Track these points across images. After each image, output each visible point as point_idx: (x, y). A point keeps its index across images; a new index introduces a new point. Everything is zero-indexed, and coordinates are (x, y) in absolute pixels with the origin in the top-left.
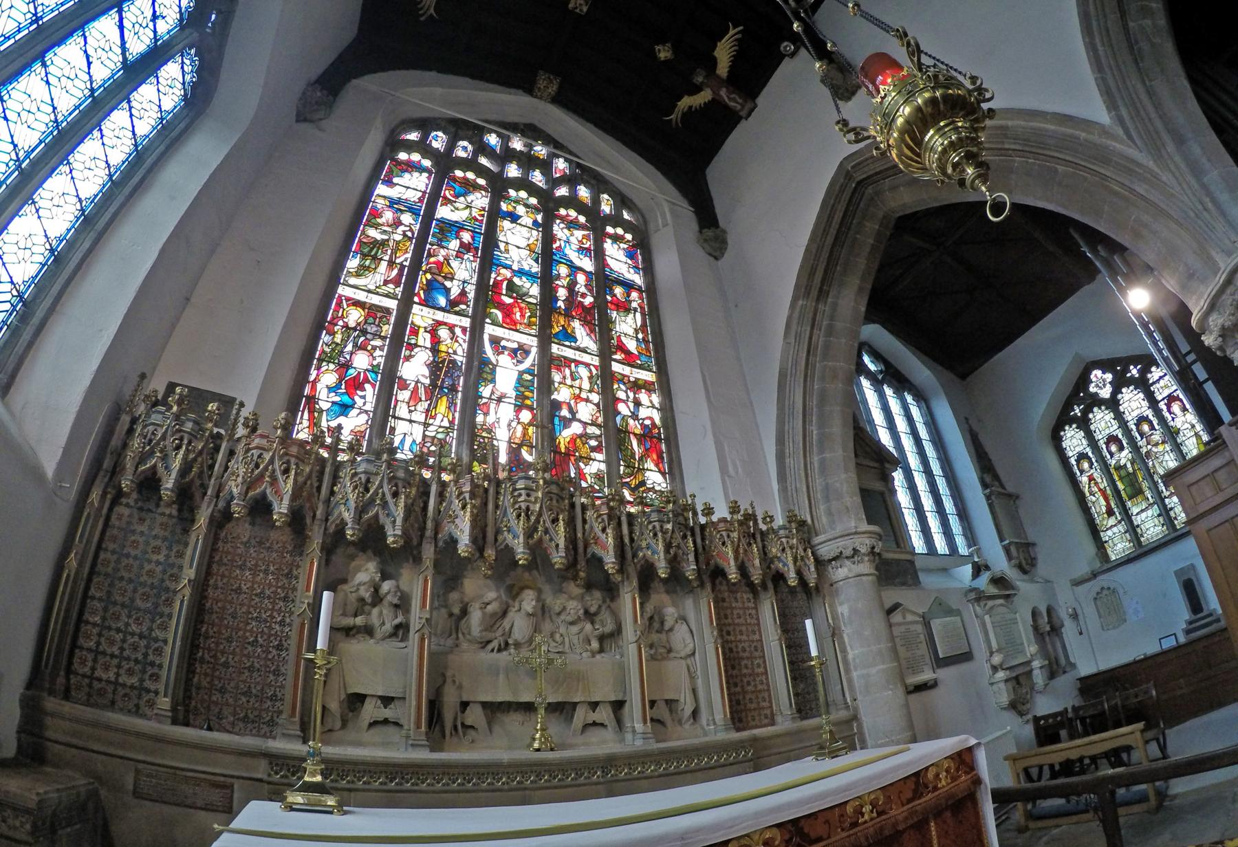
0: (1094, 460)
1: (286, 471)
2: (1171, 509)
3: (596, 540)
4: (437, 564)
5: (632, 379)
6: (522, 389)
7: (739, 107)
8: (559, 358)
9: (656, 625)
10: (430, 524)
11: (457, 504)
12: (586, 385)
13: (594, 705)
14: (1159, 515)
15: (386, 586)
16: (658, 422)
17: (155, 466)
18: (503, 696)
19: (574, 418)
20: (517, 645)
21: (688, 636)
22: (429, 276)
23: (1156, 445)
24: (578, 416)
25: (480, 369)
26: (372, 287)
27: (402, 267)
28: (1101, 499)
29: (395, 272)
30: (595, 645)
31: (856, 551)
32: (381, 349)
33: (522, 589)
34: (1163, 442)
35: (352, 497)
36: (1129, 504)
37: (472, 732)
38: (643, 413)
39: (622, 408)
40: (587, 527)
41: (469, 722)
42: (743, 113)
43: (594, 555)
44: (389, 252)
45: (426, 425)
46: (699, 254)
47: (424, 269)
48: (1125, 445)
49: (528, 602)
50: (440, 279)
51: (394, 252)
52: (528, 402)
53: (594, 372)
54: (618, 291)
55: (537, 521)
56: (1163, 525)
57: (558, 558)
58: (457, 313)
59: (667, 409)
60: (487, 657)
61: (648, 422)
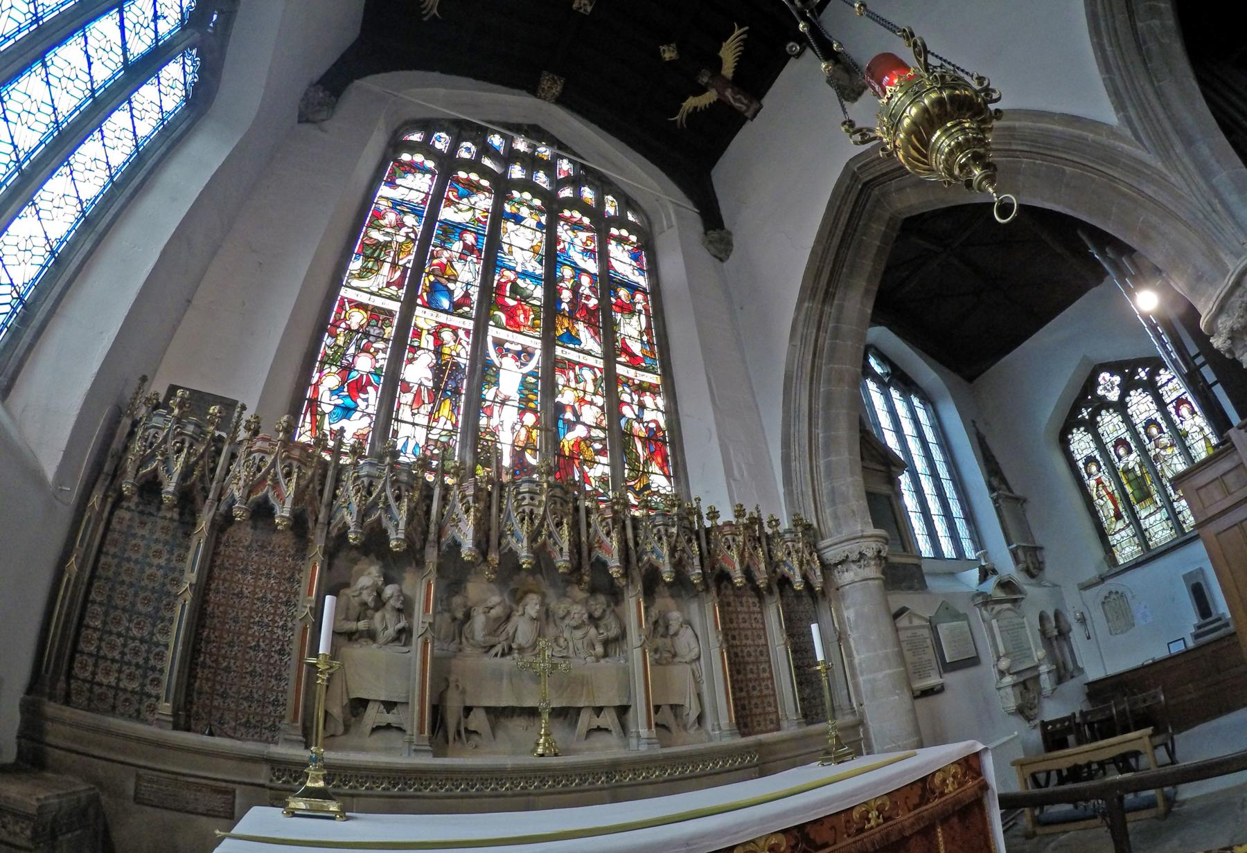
0: (1102, 463)
1: (288, 475)
2: (1180, 512)
3: (601, 543)
4: (440, 568)
5: (637, 382)
6: (526, 392)
7: (744, 108)
8: (563, 360)
9: (661, 630)
10: (433, 528)
11: (460, 507)
12: (590, 388)
13: (598, 710)
14: (1167, 519)
15: (389, 590)
16: (662, 424)
17: (156, 469)
18: (507, 701)
19: (578, 421)
20: (521, 650)
21: (693, 641)
22: (432, 278)
23: (1165, 448)
24: (582, 419)
25: (484, 372)
26: (375, 289)
27: (405, 269)
28: (1109, 503)
29: (398, 274)
30: (599, 649)
31: (862, 555)
32: (384, 351)
33: (526, 593)
34: (1172, 445)
35: (355, 501)
36: (1137, 507)
37: (475, 737)
38: (648, 416)
39: (626, 411)
40: (591, 530)
41: (472, 727)
42: (748, 114)
43: (598, 559)
44: (392, 254)
45: (429, 428)
46: (704, 256)
47: (427, 271)
48: (1133, 448)
49: (532, 606)
50: (443, 280)
51: (397, 254)
52: (532, 405)
53: (599, 374)
54: (623, 293)
55: (541, 525)
56: (1171, 529)
57: (562, 562)
58: (460, 316)
59: (672, 412)
60: (490, 662)
61: (652, 425)
